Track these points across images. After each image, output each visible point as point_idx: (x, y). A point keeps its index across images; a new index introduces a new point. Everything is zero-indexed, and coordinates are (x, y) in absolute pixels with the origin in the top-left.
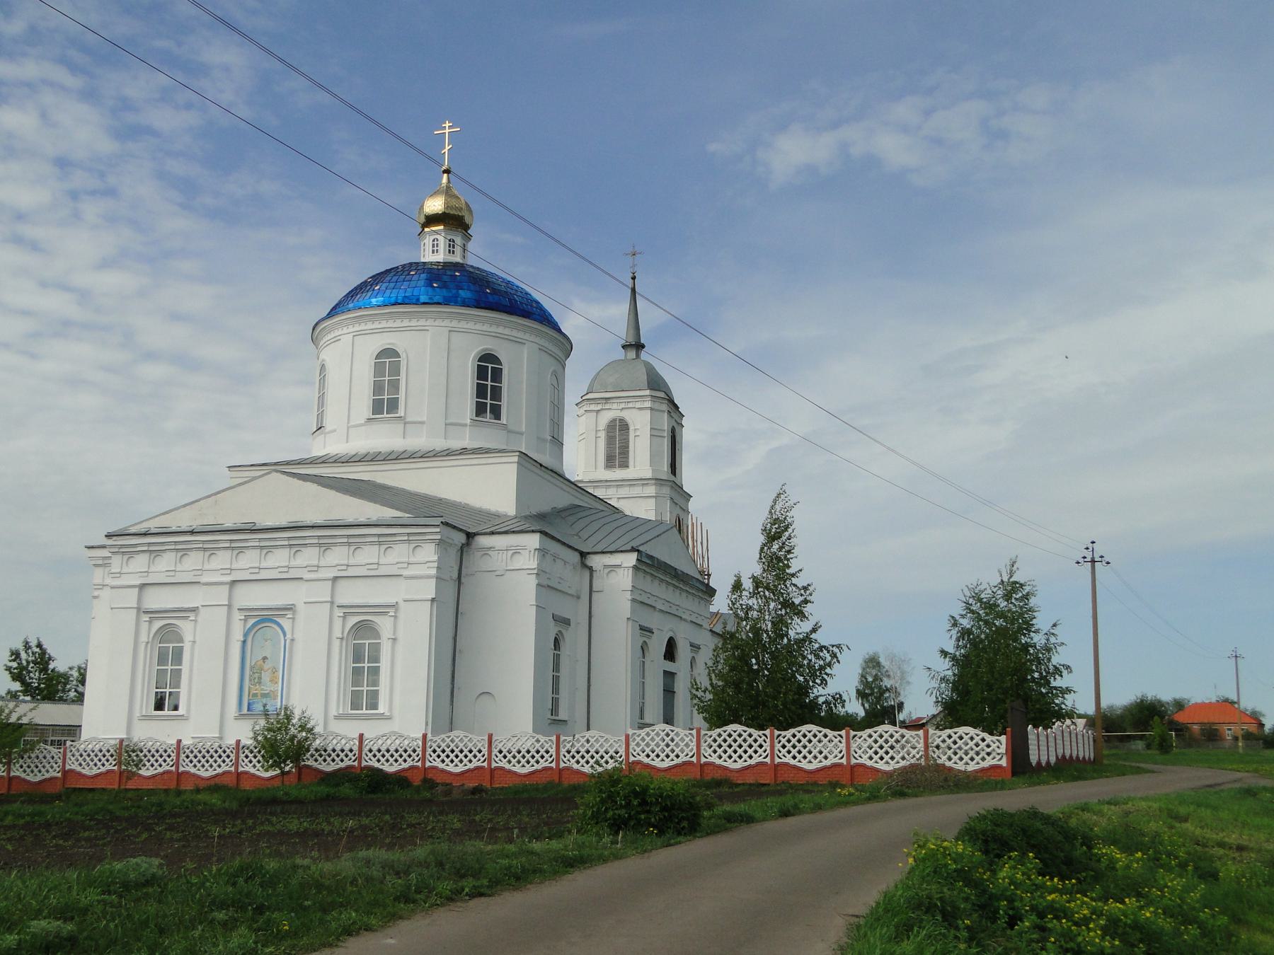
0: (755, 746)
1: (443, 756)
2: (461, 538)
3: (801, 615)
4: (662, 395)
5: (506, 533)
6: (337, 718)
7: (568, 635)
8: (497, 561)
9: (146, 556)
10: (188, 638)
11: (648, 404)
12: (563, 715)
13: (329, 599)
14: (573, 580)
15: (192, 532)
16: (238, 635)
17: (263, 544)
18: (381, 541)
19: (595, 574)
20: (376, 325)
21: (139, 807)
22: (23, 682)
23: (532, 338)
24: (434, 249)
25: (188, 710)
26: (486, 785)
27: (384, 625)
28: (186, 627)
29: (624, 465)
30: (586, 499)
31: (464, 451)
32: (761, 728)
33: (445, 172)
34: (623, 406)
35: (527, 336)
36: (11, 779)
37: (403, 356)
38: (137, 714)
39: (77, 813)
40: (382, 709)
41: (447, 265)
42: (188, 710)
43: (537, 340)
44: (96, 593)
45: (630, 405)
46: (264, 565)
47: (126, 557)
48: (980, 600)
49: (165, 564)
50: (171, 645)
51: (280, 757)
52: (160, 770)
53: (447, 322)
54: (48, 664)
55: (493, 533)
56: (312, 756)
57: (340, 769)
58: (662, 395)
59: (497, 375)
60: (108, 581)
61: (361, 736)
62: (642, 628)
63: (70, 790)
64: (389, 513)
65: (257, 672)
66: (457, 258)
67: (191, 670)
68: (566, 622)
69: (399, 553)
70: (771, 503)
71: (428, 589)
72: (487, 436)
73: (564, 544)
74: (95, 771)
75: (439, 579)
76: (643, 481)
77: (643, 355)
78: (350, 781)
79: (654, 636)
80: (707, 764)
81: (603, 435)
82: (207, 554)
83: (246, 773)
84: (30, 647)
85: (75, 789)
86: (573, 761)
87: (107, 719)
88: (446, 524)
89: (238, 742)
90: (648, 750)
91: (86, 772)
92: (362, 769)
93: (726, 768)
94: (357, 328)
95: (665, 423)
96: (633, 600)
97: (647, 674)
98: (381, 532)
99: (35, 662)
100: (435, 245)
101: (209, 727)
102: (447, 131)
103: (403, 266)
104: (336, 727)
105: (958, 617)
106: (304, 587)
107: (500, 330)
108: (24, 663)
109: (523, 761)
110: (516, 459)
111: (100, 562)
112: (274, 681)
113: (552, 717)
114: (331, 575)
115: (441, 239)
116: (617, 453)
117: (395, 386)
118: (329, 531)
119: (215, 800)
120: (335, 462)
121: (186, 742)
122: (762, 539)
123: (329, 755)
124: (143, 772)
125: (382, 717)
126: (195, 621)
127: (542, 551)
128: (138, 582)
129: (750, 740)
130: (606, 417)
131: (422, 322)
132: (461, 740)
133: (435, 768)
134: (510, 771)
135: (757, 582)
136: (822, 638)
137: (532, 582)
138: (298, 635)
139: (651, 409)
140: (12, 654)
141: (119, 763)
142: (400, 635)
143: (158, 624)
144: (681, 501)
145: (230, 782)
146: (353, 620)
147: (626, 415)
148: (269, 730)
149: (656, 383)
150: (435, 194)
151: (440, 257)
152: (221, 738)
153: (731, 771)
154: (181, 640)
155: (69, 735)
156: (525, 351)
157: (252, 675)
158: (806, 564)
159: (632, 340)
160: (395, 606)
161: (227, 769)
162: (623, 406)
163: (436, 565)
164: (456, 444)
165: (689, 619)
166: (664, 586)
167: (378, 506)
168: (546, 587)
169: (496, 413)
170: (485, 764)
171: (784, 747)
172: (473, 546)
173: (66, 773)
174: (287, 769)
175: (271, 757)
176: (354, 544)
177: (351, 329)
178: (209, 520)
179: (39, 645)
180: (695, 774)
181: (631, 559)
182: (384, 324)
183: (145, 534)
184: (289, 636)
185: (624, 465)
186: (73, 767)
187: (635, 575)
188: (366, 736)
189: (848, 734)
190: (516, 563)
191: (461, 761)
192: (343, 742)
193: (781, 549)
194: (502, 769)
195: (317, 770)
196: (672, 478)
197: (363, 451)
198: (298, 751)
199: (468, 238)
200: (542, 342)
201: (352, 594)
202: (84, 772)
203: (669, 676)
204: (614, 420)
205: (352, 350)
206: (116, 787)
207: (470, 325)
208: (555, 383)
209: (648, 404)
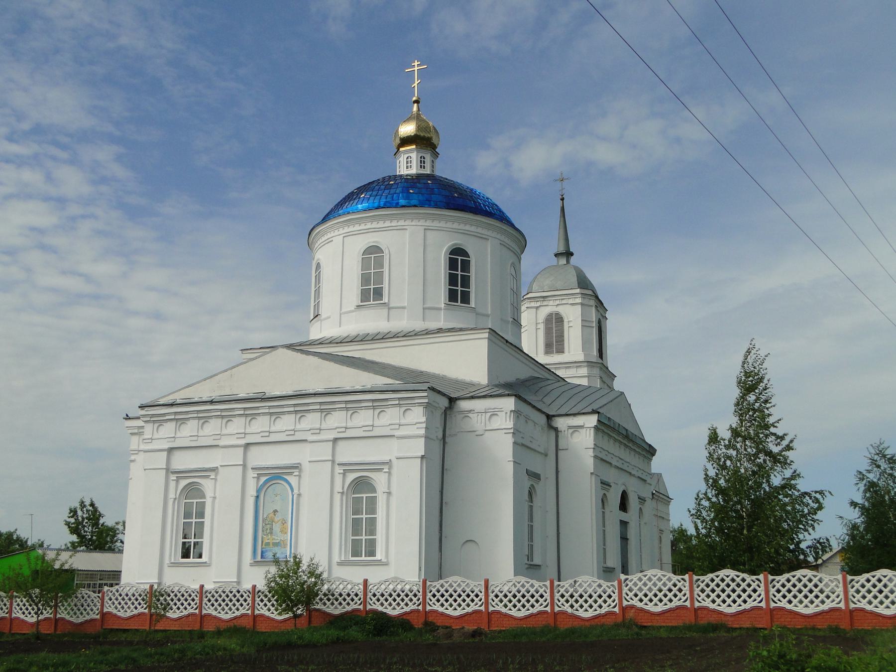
0: (749, 590)
1: (442, 600)
2: (445, 403)
3: (785, 463)
4: (590, 292)
5: (484, 397)
6: (340, 564)
7: (539, 487)
8: (477, 422)
9: (173, 424)
10: (209, 494)
11: (579, 300)
12: (537, 561)
13: (330, 458)
14: (542, 440)
15: (212, 402)
16: (251, 491)
17: (271, 411)
18: (375, 405)
19: (560, 434)
20: (363, 227)
21: (162, 654)
22: (79, 535)
23: (494, 234)
24: (408, 164)
25: (210, 557)
26: (484, 627)
27: (379, 480)
28: (207, 485)
29: (561, 351)
30: (543, 373)
31: (440, 331)
32: (753, 572)
33: (415, 102)
34: (558, 302)
35: (489, 233)
36: (57, 621)
37: (386, 251)
38: (167, 561)
39: (101, 663)
40: (379, 556)
41: (419, 177)
42: (210, 557)
43: (499, 236)
44: (133, 458)
45: (564, 302)
46: (273, 429)
47: (156, 425)
48: (884, 456)
49: (189, 429)
50: (195, 501)
51: (292, 601)
52: (185, 613)
53: (422, 222)
54: (98, 519)
55: (472, 398)
56: (321, 600)
57: (347, 613)
58: (590, 292)
59: (466, 266)
60: (142, 447)
61: (366, 581)
62: (603, 483)
63: (106, 635)
64: (380, 381)
65: (269, 524)
66: (428, 171)
67: (212, 523)
68: (535, 476)
69: (390, 416)
70: (742, 359)
71: (418, 448)
72: (458, 317)
73: (534, 407)
74: (129, 614)
75: (427, 437)
76: (577, 364)
77: (573, 260)
78: (356, 624)
79: (612, 490)
80: (700, 608)
81: (542, 327)
82: (225, 420)
83: (262, 616)
84: (85, 506)
85: (112, 630)
86: (567, 605)
87: (142, 564)
88: (432, 389)
89: (254, 587)
90: (640, 595)
91: (121, 614)
92: (368, 612)
93: (720, 613)
94: (346, 230)
95: (593, 316)
96: (596, 457)
97: (607, 523)
98: (376, 399)
99: (89, 519)
100: (409, 162)
101: (228, 573)
102: (416, 68)
103: (384, 178)
104: (339, 572)
105: (864, 473)
106: (307, 447)
107: (468, 227)
108: (80, 519)
109: (519, 605)
110: (486, 335)
111: (136, 431)
112: (283, 531)
113: (528, 565)
114: (332, 437)
115: (414, 155)
116: (555, 338)
117: (379, 276)
118: (329, 399)
119: (233, 644)
120: (330, 343)
121: (208, 587)
122: (736, 392)
123: (337, 600)
124: (170, 614)
125: (379, 563)
126: (216, 479)
127: (517, 413)
128: (166, 446)
129: (744, 585)
130: (544, 312)
131: (401, 223)
132: (459, 585)
133: (436, 612)
134: (506, 615)
135: (735, 433)
136: (803, 485)
137: (509, 440)
138: (304, 491)
139: (582, 304)
140: (71, 511)
141: (150, 607)
142: (394, 490)
143: (183, 483)
144: (605, 379)
145: (247, 624)
146: (351, 477)
147: (562, 310)
148: (281, 577)
149: (584, 283)
150: (408, 120)
151: (414, 171)
152: (238, 583)
153: (726, 615)
154: (204, 496)
155: (114, 579)
156: (489, 246)
157: (264, 524)
158: (786, 414)
159: (562, 249)
160: (389, 463)
161: (244, 612)
162: (558, 302)
163: (424, 425)
164: (433, 325)
165: (637, 474)
166: (617, 444)
167: (371, 375)
168: (521, 446)
169: (466, 298)
170: (483, 608)
171: (779, 591)
172: (455, 410)
173: (104, 615)
174: (299, 612)
175: (284, 602)
176: (352, 408)
177: (341, 231)
178: (226, 391)
179: (92, 505)
180: (689, 619)
181: (592, 420)
182: (369, 226)
183: (172, 405)
184: (296, 491)
185: (561, 351)
186: (110, 610)
187: (596, 434)
188: (370, 581)
189: (766, 578)
190: (494, 425)
191: (460, 605)
192: (349, 587)
193: (758, 399)
194: (499, 612)
195: (325, 613)
196: (600, 361)
197: (354, 334)
198: (309, 595)
199: (436, 155)
200: (503, 238)
201: (349, 453)
202: (119, 614)
203: (624, 524)
204: (550, 315)
205: (340, 251)
206: (147, 628)
207: (442, 224)
208: (514, 274)
209: (579, 300)
